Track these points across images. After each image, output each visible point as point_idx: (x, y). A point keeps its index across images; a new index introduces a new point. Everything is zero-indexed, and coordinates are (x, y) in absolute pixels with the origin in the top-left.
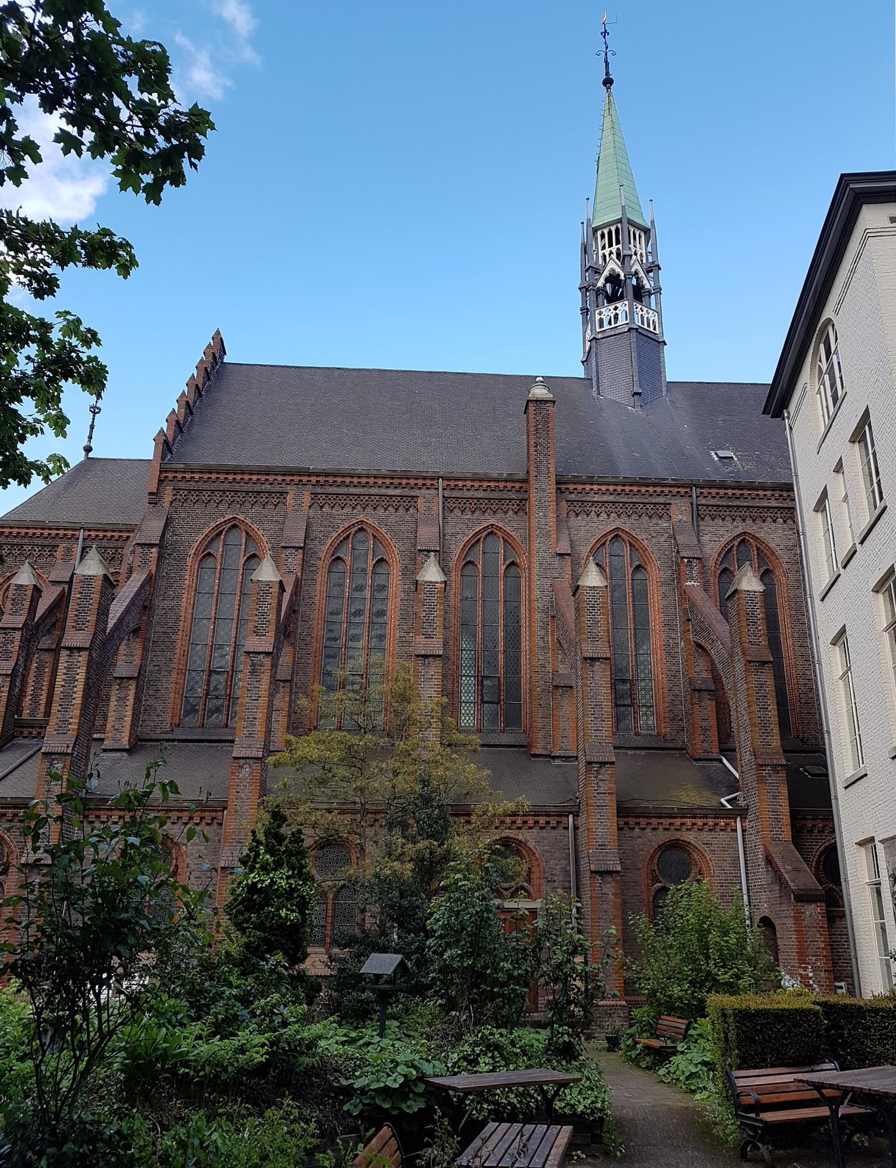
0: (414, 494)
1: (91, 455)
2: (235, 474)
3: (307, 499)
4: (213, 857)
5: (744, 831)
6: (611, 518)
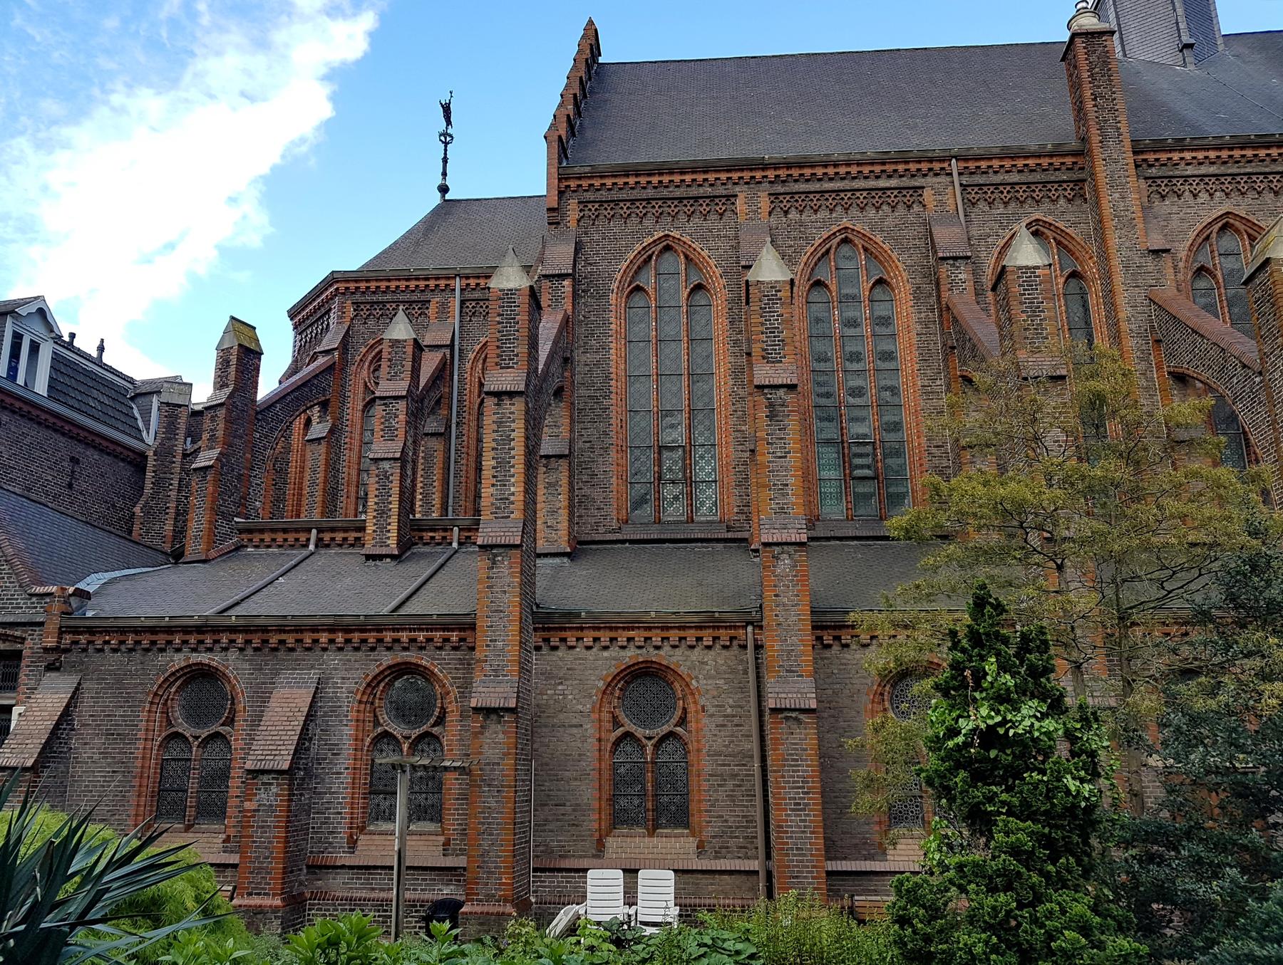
0: (917, 184)
1: (448, 197)
2: (661, 174)
3: (764, 202)
4: (740, 695)
6: (1216, 199)
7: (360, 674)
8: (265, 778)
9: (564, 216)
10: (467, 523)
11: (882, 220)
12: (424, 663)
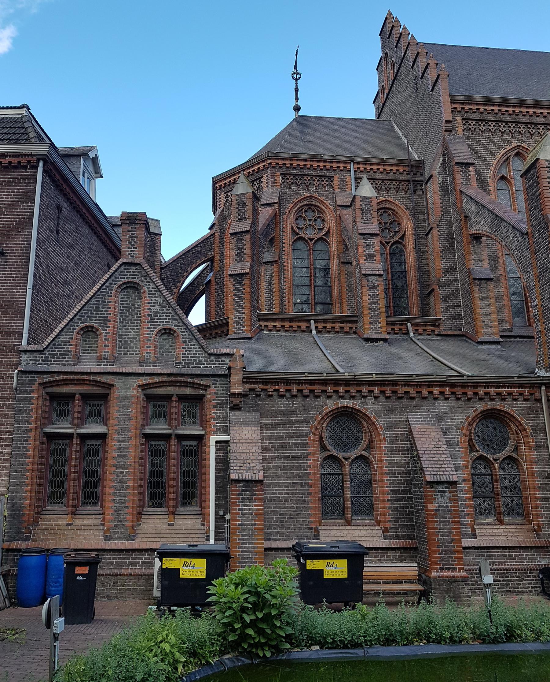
1: (300, 113)
2: (514, 107)
7: (462, 416)
8: (440, 487)
9: (454, 126)
10: (417, 320)
12: (506, 409)
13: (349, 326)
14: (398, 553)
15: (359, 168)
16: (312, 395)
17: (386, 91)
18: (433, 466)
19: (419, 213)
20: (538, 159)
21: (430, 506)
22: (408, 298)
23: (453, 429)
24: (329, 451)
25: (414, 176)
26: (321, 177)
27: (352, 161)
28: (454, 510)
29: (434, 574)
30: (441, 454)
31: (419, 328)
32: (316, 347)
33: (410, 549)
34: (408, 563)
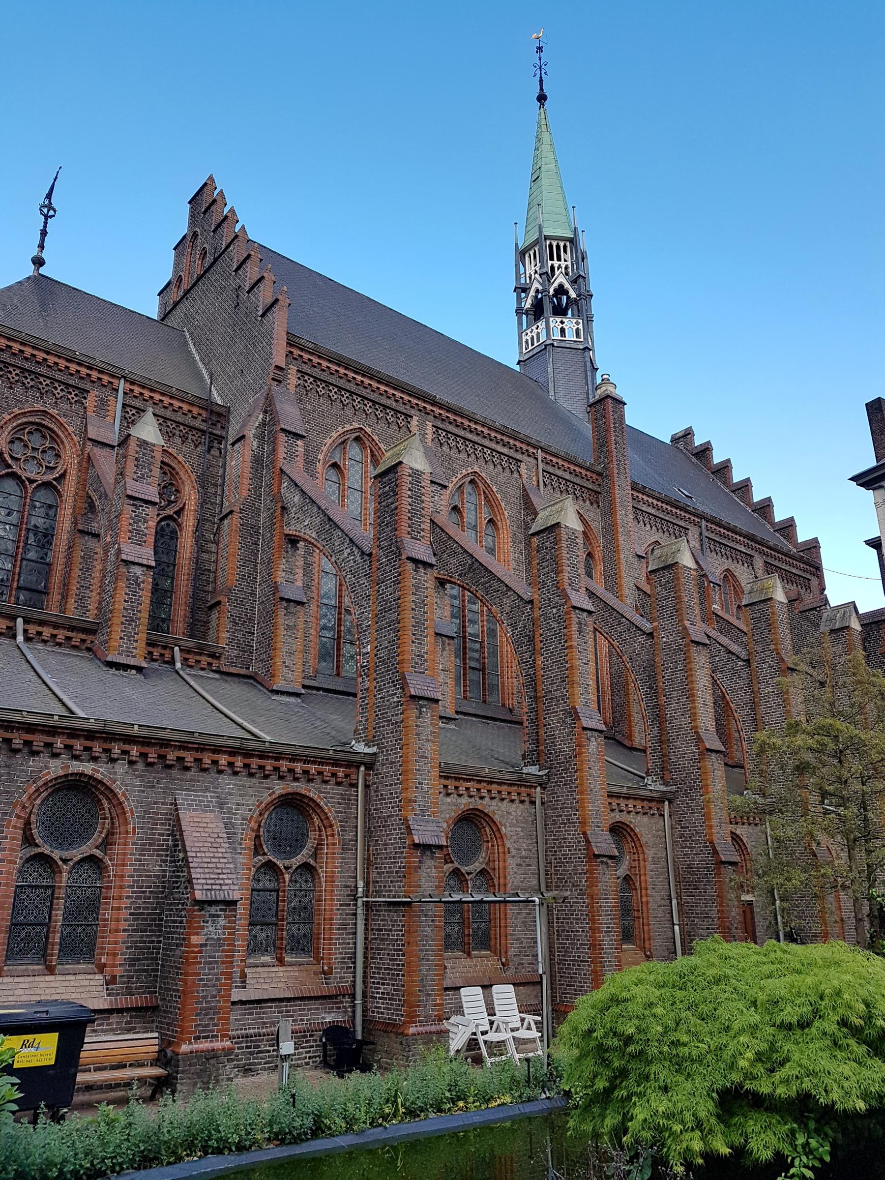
1: (42, 270)
5: (367, 786)
7: (252, 801)
8: (213, 910)
9: (285, 377)
11: (498, 474)
12: (311, 795)
13: (83, 637)
14: (127, 1017)
15: (132, 390)
16: (26, 750)
17: (185, 286)
18: (207, 876)
19: (210, 483)
20: (401, 463)
21: (194, 939)
22: (171, 605)
23: (236, 819)
24: (37, 846)
25: (209, 426)
26: (68, 385)
27: (123, 376)
28: (229, 945)
29: (185, 1048)
30: (219, 858)
31: (191, 656)
32: (26, 666)
33: (146, 1009)
34: (139, 1032)
